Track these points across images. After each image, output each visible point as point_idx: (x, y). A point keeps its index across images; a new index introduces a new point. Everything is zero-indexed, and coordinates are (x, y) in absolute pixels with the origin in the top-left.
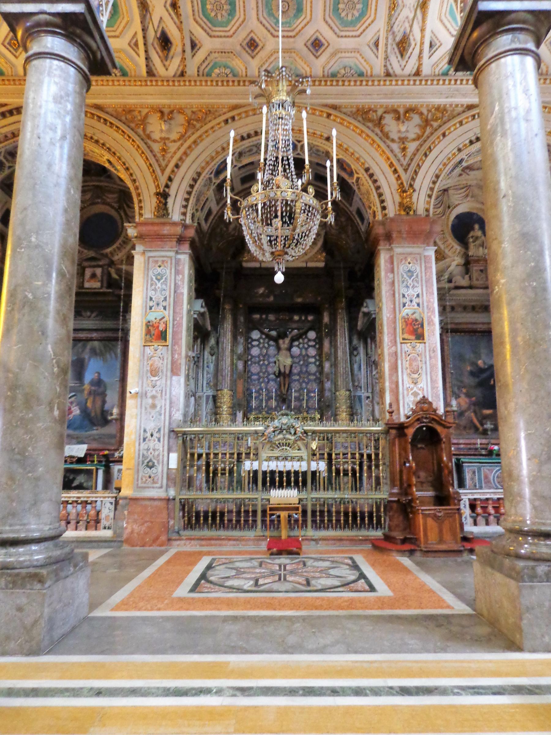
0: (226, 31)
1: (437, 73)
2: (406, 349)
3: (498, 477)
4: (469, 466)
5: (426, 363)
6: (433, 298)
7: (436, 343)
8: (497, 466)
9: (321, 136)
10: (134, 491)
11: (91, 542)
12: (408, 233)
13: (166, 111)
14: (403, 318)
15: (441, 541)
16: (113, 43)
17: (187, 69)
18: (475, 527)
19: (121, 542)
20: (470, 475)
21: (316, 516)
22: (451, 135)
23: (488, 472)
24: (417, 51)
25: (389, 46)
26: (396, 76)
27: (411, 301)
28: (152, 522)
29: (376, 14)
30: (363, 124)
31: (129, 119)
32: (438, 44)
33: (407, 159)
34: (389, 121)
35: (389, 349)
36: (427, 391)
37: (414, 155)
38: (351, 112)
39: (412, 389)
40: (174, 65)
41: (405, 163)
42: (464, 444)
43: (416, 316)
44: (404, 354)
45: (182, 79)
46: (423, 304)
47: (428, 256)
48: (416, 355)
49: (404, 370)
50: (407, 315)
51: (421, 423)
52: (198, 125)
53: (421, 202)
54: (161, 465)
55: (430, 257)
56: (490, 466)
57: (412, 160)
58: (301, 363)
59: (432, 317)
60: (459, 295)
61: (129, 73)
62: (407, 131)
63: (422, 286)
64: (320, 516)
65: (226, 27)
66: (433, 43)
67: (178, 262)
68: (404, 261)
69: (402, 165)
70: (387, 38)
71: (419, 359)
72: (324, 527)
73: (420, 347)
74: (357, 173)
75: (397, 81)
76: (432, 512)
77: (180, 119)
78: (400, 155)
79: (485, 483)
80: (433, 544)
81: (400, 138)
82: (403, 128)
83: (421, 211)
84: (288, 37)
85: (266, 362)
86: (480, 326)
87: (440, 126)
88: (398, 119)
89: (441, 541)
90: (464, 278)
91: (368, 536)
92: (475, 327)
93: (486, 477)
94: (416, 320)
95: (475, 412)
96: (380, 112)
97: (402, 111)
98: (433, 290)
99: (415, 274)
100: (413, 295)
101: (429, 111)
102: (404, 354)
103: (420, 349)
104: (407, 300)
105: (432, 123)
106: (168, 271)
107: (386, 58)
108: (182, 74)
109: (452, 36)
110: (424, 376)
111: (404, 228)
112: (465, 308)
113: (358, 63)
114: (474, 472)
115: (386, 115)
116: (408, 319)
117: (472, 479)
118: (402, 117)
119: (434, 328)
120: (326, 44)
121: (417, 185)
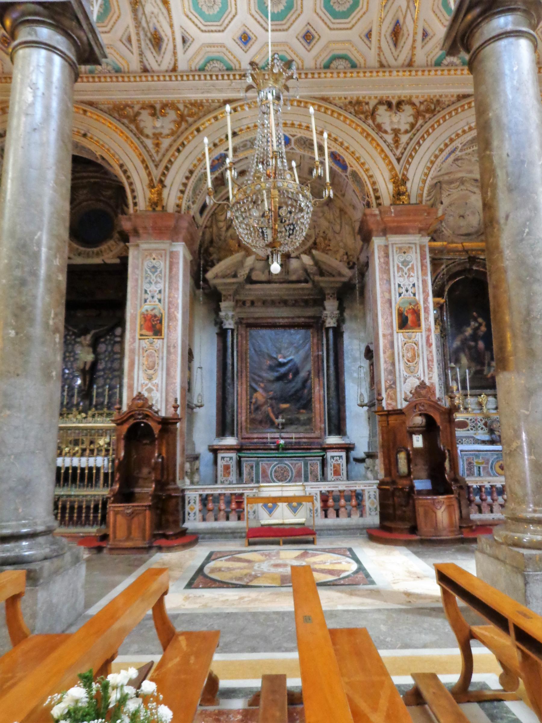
0: (217, 26)
1: (193, 68)
2: (144, 345)
3: (275, 471)
4: (247, 461)
5: (162, 359)
6: (178, 294)
7: (177, 339)
8: (275, 460)
9: (79, 132)
12: (154, 228)
13: (394, 102)
14: (142, 314)
15: (128, 537)
16: (104, 39)
17: (416, 59)
20: (248, 469)
22: (206, 130)
23: (266, 466)
24: (171, 47)
25: (143, 42)
26: (389, 66)
27: (153, 297)
29: (119, 9)
30: (119, 121)
31: (124, 114)
32: (191, 39)
33: (160, 154)
34: (145, 118)
35: (130, 345)
36: (162, 386)
37: (167, 150)
38: (108, 108)
39: (146, 385)
40: (404, 55)
41: (398, 153)
42: (257, 438)
43: (156, 312)
44: (141, 351)
45: (202, 74)
46: (164, 300)
47: (176, 252)
48: (153, 351)
49: (141, 367)
50: (147, 311)
51: (135, 419)
52: (427, 116)
53: (171, 198)
55: (177, 253)
56: (268, 461)
57: (164, 155)
58: (107, 359)
59: (176, 313)
60: (255, 290)
61: (358, 65)
62: (162, 127)
63: (165, 282)
65: (282, 20)
66: (186, 39)
67: (173, 255)
68: (148, 257)
69: (153, 161)
70: (138, 34)
71: (156, 355)
73: (158, 343)
74: (351, 166)
75: (152, 76)
77: (408, 110)
78: (153, 151)
79: (263, 477)
80: (120, 541)
81: (154, 134)
82: (158, 124)
83: (171, 208)
84: (277, 30)
85: (72, 359)
86: (281, 320)
87: (195, 121)
88: (154, 115)
90: (263, 273)
91: (89, 533)
92: (276, 321)
93: (264, 471)
94: (155, 316)
95: (272, 406)
96: (136, 108)
97: (158, 106)
98: (178, 286)
99: (159, 270)
100: (156, 291)
101: (186, 106)
102: (141, 351)
103: (158, 345)
104: (148, 296)
105: (188, 118)
106: (162, 264)
107: (141, 54)
108: (174, 69)
109: (445, 26)
110: (159, 372)
111: (149, 223)
112: (264, 303)
113: (115, 60)
114: (252, 467)
115: (142, 111)
116: (147, 315)
117: (250, 474)
118: (158, 112)
119: (177, 324)
120: (317, 37)
121: (167, 182)
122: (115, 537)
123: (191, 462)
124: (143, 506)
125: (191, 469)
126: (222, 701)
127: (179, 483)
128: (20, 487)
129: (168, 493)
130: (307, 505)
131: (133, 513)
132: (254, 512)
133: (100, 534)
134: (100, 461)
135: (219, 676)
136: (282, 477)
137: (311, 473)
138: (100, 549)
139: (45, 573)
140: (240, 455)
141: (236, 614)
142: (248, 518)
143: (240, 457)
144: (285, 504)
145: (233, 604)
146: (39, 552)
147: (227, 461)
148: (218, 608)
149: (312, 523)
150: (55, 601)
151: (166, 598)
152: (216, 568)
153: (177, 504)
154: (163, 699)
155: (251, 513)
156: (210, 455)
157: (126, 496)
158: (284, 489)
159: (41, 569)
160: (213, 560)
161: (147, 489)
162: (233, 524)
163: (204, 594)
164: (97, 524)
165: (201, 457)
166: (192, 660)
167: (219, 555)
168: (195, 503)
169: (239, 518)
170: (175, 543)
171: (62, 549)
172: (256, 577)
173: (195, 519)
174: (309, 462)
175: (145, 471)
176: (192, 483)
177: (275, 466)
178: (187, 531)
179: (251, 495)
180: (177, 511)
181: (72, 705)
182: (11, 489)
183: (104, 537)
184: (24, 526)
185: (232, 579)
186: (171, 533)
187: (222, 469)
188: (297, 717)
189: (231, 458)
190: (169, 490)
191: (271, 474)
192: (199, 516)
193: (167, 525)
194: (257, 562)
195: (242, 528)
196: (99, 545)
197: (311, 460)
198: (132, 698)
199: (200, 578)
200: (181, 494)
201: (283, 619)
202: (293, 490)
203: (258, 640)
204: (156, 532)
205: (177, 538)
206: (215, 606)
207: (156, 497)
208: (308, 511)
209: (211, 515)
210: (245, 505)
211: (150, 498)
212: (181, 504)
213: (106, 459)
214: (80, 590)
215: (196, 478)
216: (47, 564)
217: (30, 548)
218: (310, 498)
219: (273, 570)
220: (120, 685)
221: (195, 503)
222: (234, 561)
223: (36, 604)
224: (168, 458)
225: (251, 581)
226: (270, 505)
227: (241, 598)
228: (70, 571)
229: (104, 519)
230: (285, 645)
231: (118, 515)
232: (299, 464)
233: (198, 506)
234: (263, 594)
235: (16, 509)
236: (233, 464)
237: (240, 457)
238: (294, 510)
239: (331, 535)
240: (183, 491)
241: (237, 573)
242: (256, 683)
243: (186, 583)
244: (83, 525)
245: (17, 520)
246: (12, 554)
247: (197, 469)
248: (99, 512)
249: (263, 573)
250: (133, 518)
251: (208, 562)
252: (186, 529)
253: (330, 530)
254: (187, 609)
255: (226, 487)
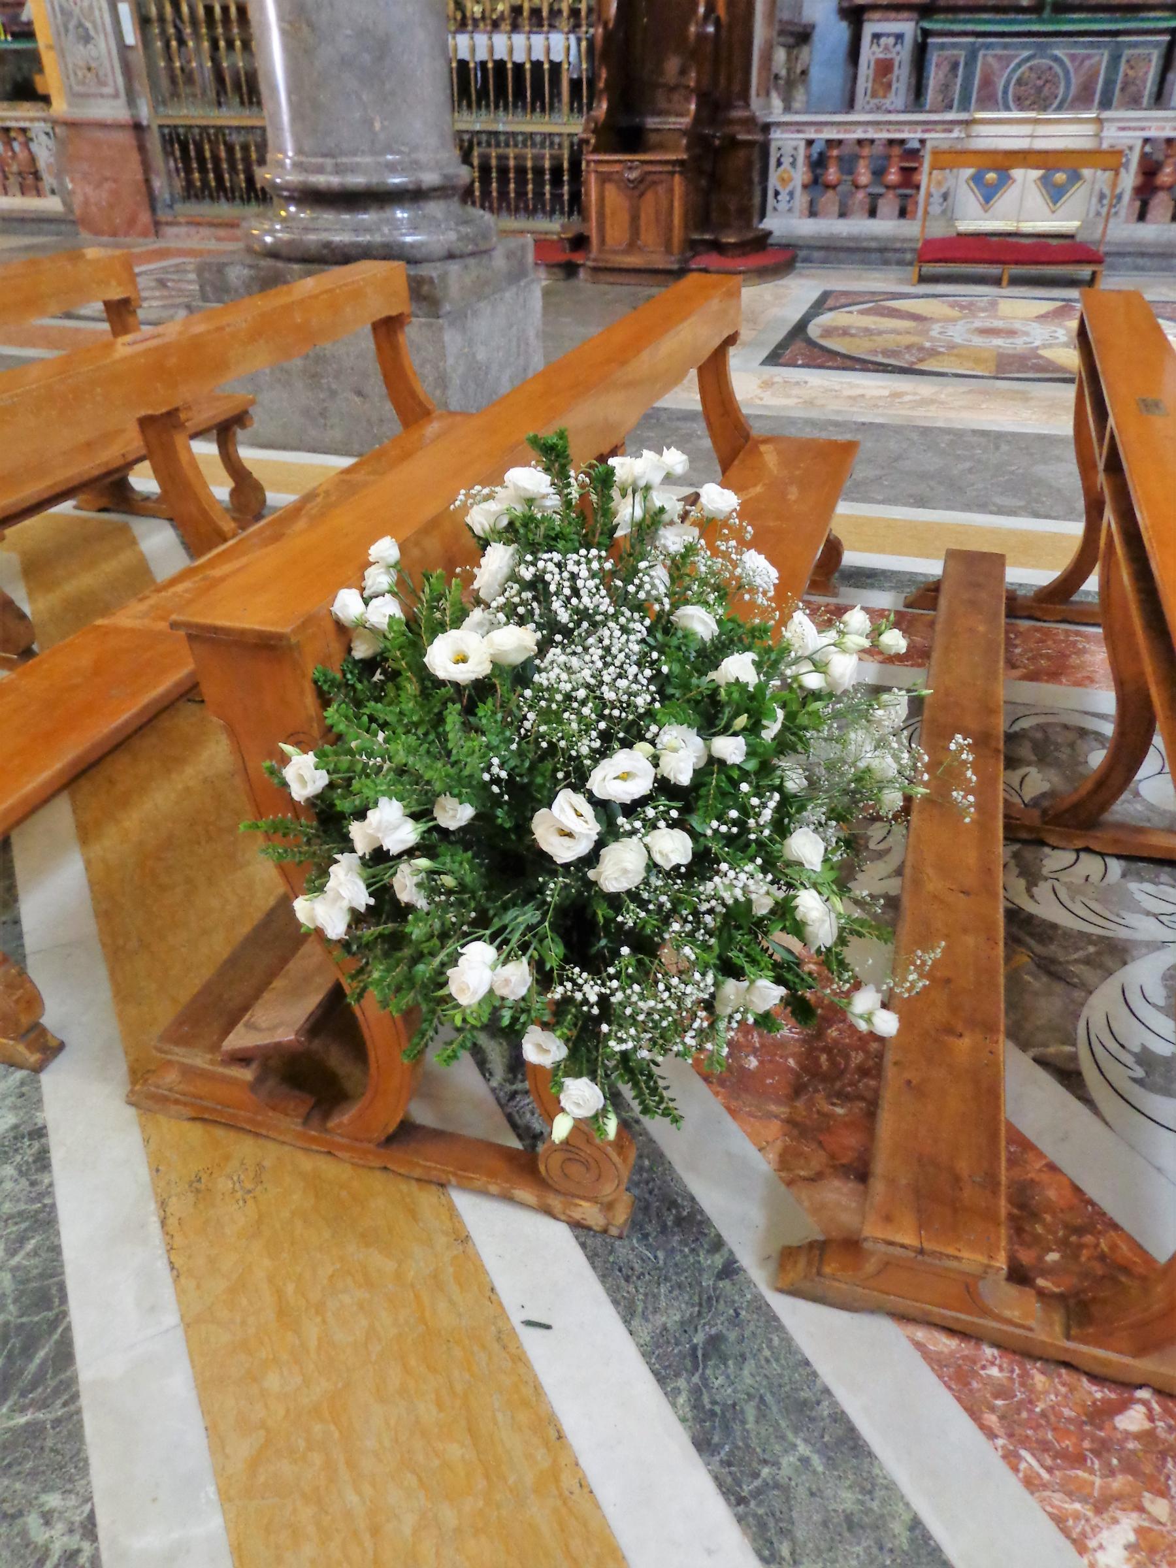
3: (1019, 82)
4: (942, 46)
8: (1024, 46)
10: (70, 105)
11: (22, 220)
15: (632, 246)
18: (811, 221)
19: (73, 222)
20: (941, 75)
21: (526, 183)
28: (115, 181)
54: (102, 36)
56: (1006, 46)
64: (499, 180)
72: (527, 206)
76: (617, 168)
89: (632, 246)
93: (987, 82)
114: (955, 66)
117: (946, 88)
122: (602, 241)
123: (789, 48)
124: (667, 162)
125: (789, 70)
126: (844, 590)
127: (755, 102)
128: (366, 58)
129: (729, 130)
130: (1095, 178)
131: (641, 180)
132: (945, 197)
133: (569, 235)
134: (558, 46)
135: (845, 543)
136: (1036, 96)
137: (1123, 90)
138: (570, 270)
139: (454, 289)
140: (927, 25)
141: (882, 426)
142: (926, 212)
143: (926, 33)
144: (1036, 174)
145: (876, 406)
146: (435, 238)
147: (886, 48)
148: (838, 412)
149: (1097, 235)
150: (481, 356)
151: (732, 351)
152: (836, 328)
153: (749, 164)
154: (754, 536)
155: (937, 198)
156: (841, 30)
157: (624, 135)
158: (1042, 130)
159: (444, 277)
160: (831, 309)
161: (675, 119)
162: (885, 226)
163: (807, 378)
164: (562, 213)
165: (816, 37)
166: (793, 493)
167: (843, 301)
168: (793, 164)
169: (903, 213)
170: (741, 264)
171: (485, 237)
172: (933, 353)
173: (790, 210)
174: (1127, 53)
175: (672, 65)
176: (788, 109)
177: (1019, 65)
178: (771, 241)
179: (945, 146)
180: (750, 182)
181: (519, 510)
182: (345, 62)
183: (580, 242)
184: (392, 168)
185: (875, 352)
186: (732, 240)
187: (871, 72)
188: (1017, 642)
189: (899, 37)
190: (731, 122)
191: (1005, 92)
192: (801, 200)
193: (722, 216)
194: (938, 321)
195: (905, 240)
196: (569, 259)
197: (1135, 45)
198: (672, 523)
199: (799, 345)
200: (758, 137)
201: (997, 448)
202: (1065, 132)
203: (932, 483)
204: (696, 237)
205: (744, 254)
206: (834, 405)
207: (697, 139)
208: (1094, 200)
209: (829, 200)
210: (923, 178)
211: (684, 141)
212: (757, 166)
213: (572, 37)
214: (533, 341)
215: (800, 97)
216: (454, 267)
217: (415, 228)
218: (1111, 159)
219: (978, 341)
220: (642, 483)
221: (793, 164)
222: (882, 315)
223: (443, 357)
224: (730, 27)
225: (921, 360)
226: (991, 176)
227: (895, 395)
228: (508, 295)
229: (577, 202)
230: (998, 500)
231: (606, 185)
232: (1096, 59)
233: (800, 175)
234: (950, 390)
235: (368, 123)
236: (903, 55)
237: (926, 33)
238: (1055, 194)
239: (1142, 269)
240: (766, 128)
241: (890, 341)
242: (933, 568)
243: (765, 353)
244: (532, 213)
245: (373, 152)
246: (378, 238)
247: (804, 73)
248: (562, 186)
249: (952, 347)
250: (642, 195)
251: (818, 315)
252: (770, 233)
253: (1143, 255)
254: (766, 407)
255: (876, 121)
